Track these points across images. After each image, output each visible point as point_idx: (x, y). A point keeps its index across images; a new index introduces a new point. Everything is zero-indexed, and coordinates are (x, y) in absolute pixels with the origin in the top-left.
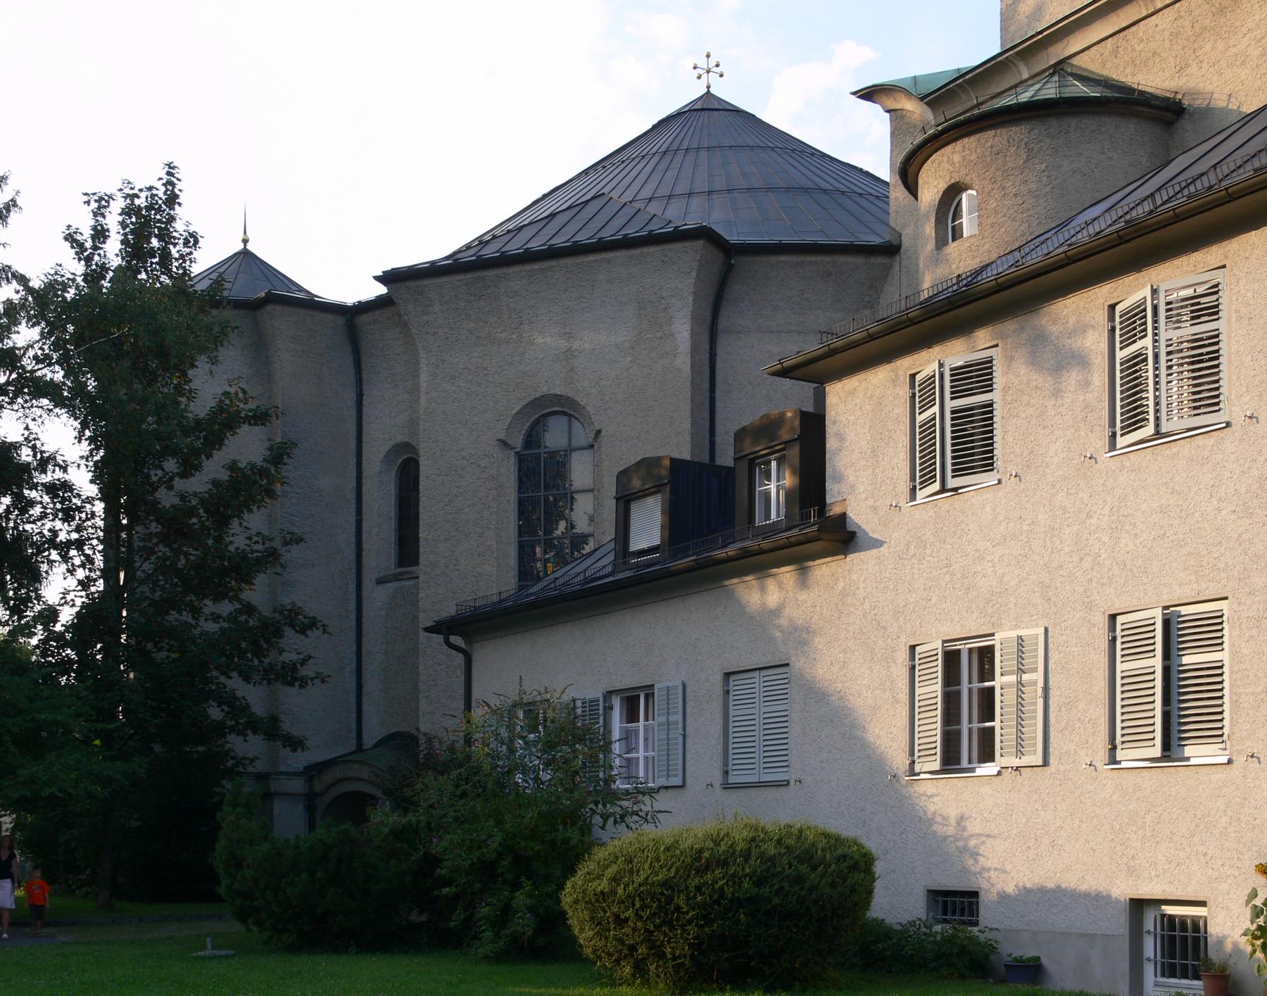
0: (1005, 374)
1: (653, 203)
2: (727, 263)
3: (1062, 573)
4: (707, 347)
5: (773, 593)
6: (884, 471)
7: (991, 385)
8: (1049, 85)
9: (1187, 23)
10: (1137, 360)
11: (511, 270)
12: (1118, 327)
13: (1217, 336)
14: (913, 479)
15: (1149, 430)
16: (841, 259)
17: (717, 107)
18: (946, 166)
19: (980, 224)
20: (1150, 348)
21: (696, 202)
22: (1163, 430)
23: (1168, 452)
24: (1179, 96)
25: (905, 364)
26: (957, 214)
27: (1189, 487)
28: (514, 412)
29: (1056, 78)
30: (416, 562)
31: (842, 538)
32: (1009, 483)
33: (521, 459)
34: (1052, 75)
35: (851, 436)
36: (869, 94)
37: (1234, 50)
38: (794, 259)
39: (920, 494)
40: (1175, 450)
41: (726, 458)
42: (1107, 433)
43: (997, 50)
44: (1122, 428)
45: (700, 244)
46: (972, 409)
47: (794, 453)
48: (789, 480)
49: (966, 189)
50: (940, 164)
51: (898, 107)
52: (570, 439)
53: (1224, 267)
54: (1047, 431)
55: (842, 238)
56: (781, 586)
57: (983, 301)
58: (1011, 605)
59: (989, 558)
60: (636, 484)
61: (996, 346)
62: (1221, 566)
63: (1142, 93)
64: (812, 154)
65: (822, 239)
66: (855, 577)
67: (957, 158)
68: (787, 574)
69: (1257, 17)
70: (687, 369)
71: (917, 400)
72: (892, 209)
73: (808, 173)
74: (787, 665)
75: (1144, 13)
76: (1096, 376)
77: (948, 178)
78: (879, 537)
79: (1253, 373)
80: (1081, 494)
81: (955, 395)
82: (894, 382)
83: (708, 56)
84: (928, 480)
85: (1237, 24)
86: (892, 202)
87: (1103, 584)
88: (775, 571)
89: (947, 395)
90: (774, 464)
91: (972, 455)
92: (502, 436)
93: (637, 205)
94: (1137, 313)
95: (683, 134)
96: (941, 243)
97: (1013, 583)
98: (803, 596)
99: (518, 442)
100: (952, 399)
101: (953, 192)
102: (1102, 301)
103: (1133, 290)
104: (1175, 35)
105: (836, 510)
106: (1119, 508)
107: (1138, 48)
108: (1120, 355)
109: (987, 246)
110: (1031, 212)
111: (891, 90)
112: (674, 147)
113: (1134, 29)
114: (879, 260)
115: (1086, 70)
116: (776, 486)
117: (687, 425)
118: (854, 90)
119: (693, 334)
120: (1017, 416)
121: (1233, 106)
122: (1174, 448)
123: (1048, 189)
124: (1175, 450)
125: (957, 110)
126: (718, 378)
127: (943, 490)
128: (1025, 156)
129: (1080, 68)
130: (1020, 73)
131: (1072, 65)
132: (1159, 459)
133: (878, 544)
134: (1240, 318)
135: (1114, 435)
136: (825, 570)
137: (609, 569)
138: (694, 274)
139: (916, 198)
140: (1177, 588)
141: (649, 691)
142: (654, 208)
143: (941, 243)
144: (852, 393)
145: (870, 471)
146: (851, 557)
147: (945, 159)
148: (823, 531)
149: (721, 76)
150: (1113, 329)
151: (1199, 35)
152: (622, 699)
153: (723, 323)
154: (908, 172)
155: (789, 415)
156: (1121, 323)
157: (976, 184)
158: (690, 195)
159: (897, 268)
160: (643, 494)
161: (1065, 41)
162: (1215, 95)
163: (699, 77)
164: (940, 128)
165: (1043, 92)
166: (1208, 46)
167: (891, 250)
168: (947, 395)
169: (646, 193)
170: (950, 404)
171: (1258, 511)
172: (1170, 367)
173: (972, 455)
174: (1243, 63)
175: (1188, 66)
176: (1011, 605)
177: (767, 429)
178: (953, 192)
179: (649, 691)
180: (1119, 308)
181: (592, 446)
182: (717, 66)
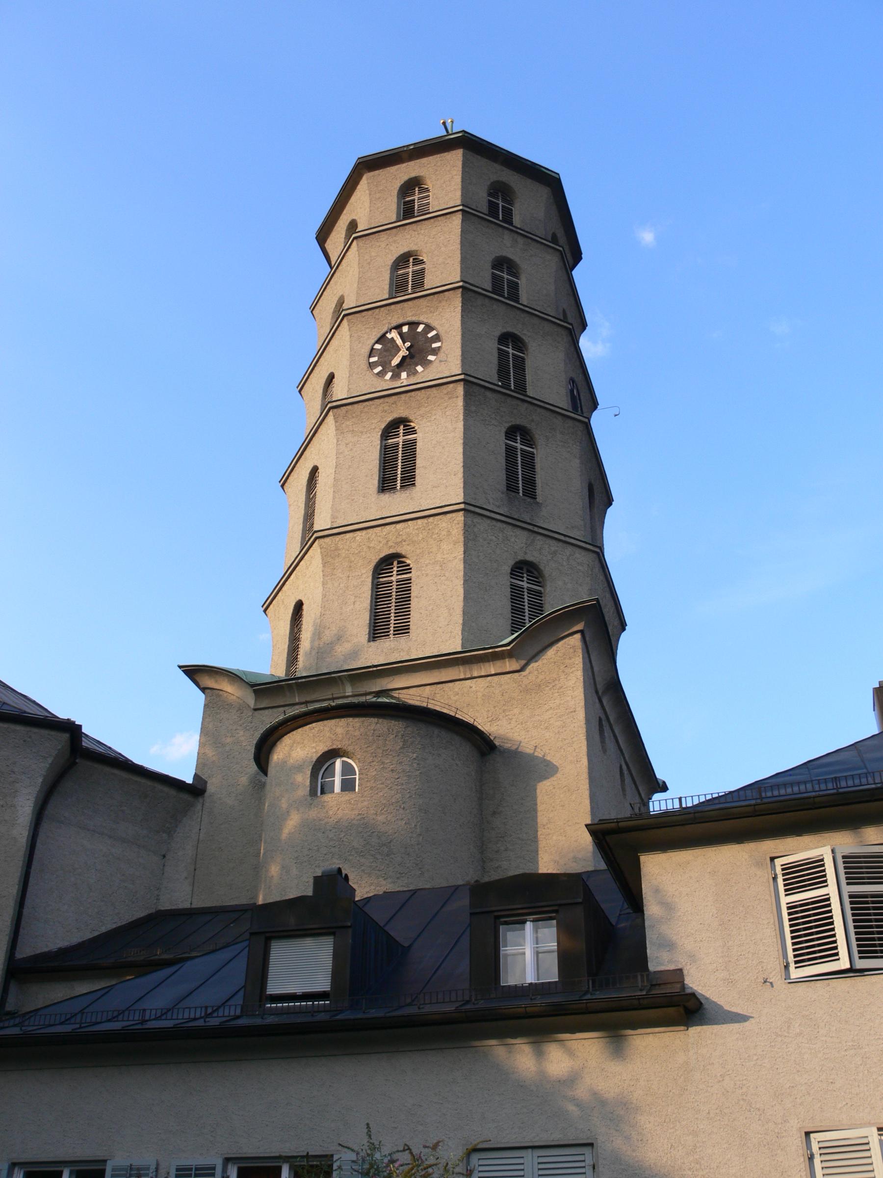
36: (193, 672)
46: (807, 904)
49: (342, 756)
57: (828, 809)
67: (339, 730)
69: (557, 701)
74: (591, 1145)
75: (462, 677)
85: (541, 702)
107: (455, 698)
109: (366, 803)
110: (404, 787)
113: (451, 684)
118: (181, 664)
128: (401, 744)
130: (344, 690)
138: (50, 760)
146: (694, 1030)
152: (71, 1173)
153: (49, 810)
161: (391, 678)
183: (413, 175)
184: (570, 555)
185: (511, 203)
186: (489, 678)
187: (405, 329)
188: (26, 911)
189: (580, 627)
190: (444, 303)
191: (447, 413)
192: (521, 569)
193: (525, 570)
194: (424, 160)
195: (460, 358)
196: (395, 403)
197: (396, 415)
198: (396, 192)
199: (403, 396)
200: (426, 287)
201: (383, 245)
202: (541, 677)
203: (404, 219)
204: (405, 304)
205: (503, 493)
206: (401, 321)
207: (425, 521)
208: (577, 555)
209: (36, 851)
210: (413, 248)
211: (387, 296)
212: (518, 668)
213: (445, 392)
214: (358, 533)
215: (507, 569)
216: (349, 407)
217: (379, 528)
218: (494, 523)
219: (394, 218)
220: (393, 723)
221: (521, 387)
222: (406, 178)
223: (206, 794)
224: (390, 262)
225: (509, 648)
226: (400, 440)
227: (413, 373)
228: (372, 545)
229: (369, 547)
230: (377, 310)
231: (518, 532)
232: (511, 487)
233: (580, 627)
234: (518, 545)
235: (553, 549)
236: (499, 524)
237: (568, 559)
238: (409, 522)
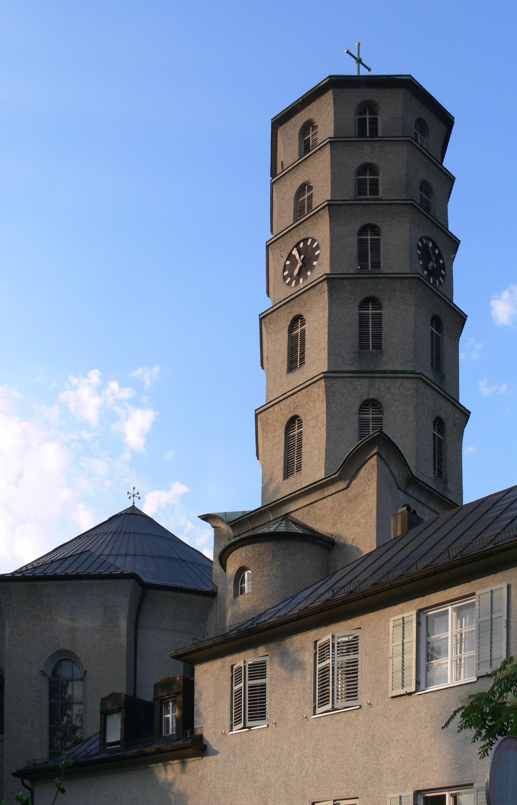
0: (271, 670)
1: (110, 557)
2: (144, 593)
3: (293, 777)
4: (134, 633)
5: (169, 773)
6: (219, 714)
7: (265, 675)
8: (281, 525)
9: (337, 504)
10: (325, 670)
12: (318, 652)
13: (357, 662)
14: (231, 720)
15: (329, 707)
16: (192, 596)
17: (138, 513)
18: (239, 558)
19: (252, 588)
20: (331, 664)
21: (129, 559)
22: (335, 707)
23: (337, 718)
24: (333, 537)
25: (229, 660)
26: (243, 582)
27: (345, 737)
28: (48, 656)
29: (284, 522)
31: (200, 748)
32: (272, 726)
33: (51, 682)
34: (282, 520)
35: (205, 694)
36: (206, 518)
37: (355, 519)
39: (235, 728)
40: (339, 718)
41: (147, 694)
42: (313, 706)
43: (259, 505)
44: (319, 704)
45: (132, 581)
46: (256, 686)
47: (180, 698)
48: (177, 713)
49: (247, 570)
50: (236, 556)
51: (218, 525)
52: (72, 675)
53: (360, 628)
54: (288, 702)
55: (193, 586)
56: (173, 770)
58: (272, 793)
59: (263, 766)
60: (110, 706)
61: (268, 655)
62: (356, 780)
63: (319, 533)
64: (178, 542)
65: (183, 585)
66: (206, 770)
67: (243, 554)
68: (176, 764)
70: (125, 644)
71: (234, 679)
72: (214, 575)
73: (177, 551)
75: (320, 498)
76: (308, 676)
77: (239, 564)
78: (217, 749)
79: (371, 682)
80: (302, 737)
81: (251, 678)
82: (223, 667)
83: (134, 489)
84: (238, 722)
85: (357, 508)
86: (214, 571)
87: (310, 786)
88: (171, 762)
89: (247, 678)
90: (171, 703)
91: (256, 710)
92: (42, 668)
93: (104, 557)
94: (325, 646)
95: (122, 525)
96: (236, 595)
97: (273, 781)
98: (184, 777)
99: (49, 672)
100: (249, 680)
101: (242, 570)
102: (311, 639)
103: (325, 635)
104: (332, 509)
105: (198, 732)
106: (317, 745)
107: (318, 513)
108: (319, 666)
110: (273, 585)
111: (215, 517)
112: (119, 530)
113: (316, 504)
114: (208, 599)
115: (296, 519)
116: (171, 715)
117: (124, 673)
119: (128, 627)
120: (276, 692)
121: (354, 545)
122: (339, 717)
123: (281, 574)
124: (339, 718)
125: (247, 531)
126: (138, 651)
127: (244, 727)
129: (294, 518)
131: (291, 517)
132: (333, 721)
133: (216, 753)
134: (366, 654)
135: (315, 707)
136: (193, 763)
137: (97, 751)
138: (129, 596)
139: (225, 571)
140: (339, 791)
142: (111, 560)
143: (236, 595)
144: (206, 671)
145: (213, 713)
146: (204, 758)
147: (239, 554)
148: (195, 746)
149: (139, 499)
150: (316, 653)
151: (342, 510)
154: (223, 557)
155: (178, 679)
156: (319, 651)
157: (251, 568)
158: (126, 555)
159: (215, 604)
160: (112, 712)
161: (288, 505)
162: (348, 539)
163: (130, 498)
164: (237, 539)
165: (279, 528)
166: (345, 516)
167: (213, 594)
168: (247, 678)
169: (107, 552)
170: (248, 683)
171: (371, 752)
172: (338, 675)
173: (256, 710)
174: (359, 526)
175: (337, 523)
176: (272, 793)
177: (166, 685)
178: (242, 570)
180: (318, 643)
181: (82, 679)
182: (138, 494)
183: (306, 119)
184: (400, 385)
185: (376, 113)
186: (333, 496)
187: (301, 245)
188: (138, 682)
189: (375, 451)
190: (320, 220)
191: (320, 305)
192: (368, 405)
193: (371, 405)
194: (310, 107)
195: (329, 259)
196: (293, 306)
197: (294, 314)
198: (297, 136)
199: (296, 299)
200: (313, 208)
201: (289, 184)
202: (357, 490)
203: (305, 155)
204: (299, 228)
205: (355, 353)
206: (298, 240)
207: (306, 390)
208: (405, 384)
209: (138, 647)
210: (306, 179)
211: (292, 222)
212: (346, 486)
213: (318, 290)
214: (276, 406)
215: (356, 409)
216: (270, 315)
217: (285, 401)
218: (345, 379)
219: (297, 156)
220: (267, 544)
221: (376, 264)
222: (301, 124)
223: (218, 595)
224: (293, 195)
225: (337, 475)
226: (299, 330)
227: (306, 278)
228: (283, 413)
229: (282, 414)
230: (285, 236)
231: (363, 381)
232: (363, 346)
233: (375, 451)
234: (363, 389)
235: (387, 385)
236: (349, 380)
237: (399, 388)
238: (299, 393)
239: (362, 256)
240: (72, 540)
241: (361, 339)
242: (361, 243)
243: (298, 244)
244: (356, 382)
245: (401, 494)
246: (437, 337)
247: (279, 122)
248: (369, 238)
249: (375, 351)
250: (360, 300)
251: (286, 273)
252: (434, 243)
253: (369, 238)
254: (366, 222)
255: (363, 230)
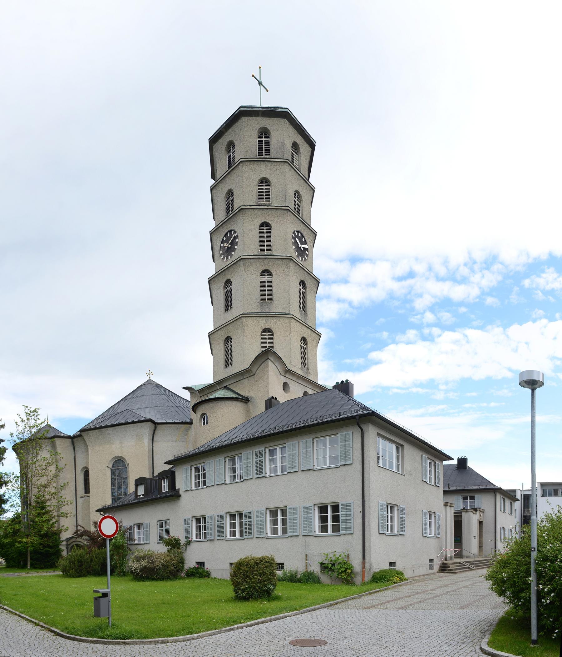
11: (108, 429)
30: (89, 493)
33: (112, 470)
38: (170, 425)
70: (147, 450)
99: (111, 466)
114: (188, 426)
115: (370, 525)
141: (142, 524)
179: (142, 524)
183: (228, 140)
187: (229, 234)
194: (230, 130)
206: (227, 231)
227: (231, 256)
231: (262, 318)
239: (262, 242)
240: (120, 401)
241: (261, 287)
242: (261, 234)
243: (227, 234)
244: (259, 319)
245: (282, 377)
246: (305, 349)
247: (214, 140)
248: (265, 231)
249: (268, 301)
250: (260, 271)
251: (221, 252)
252: (301, 234)
253: (265, 231)
254: (263, 221)
255: (264, 272)
